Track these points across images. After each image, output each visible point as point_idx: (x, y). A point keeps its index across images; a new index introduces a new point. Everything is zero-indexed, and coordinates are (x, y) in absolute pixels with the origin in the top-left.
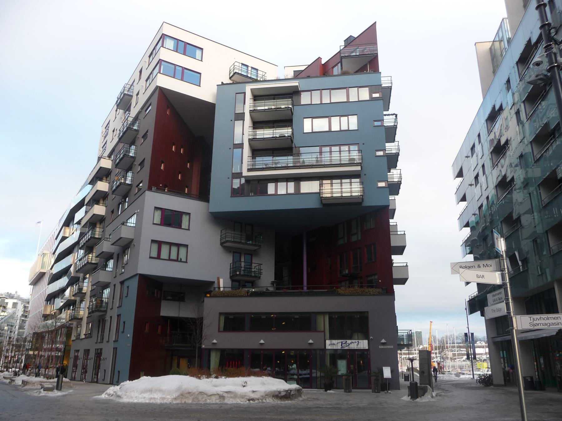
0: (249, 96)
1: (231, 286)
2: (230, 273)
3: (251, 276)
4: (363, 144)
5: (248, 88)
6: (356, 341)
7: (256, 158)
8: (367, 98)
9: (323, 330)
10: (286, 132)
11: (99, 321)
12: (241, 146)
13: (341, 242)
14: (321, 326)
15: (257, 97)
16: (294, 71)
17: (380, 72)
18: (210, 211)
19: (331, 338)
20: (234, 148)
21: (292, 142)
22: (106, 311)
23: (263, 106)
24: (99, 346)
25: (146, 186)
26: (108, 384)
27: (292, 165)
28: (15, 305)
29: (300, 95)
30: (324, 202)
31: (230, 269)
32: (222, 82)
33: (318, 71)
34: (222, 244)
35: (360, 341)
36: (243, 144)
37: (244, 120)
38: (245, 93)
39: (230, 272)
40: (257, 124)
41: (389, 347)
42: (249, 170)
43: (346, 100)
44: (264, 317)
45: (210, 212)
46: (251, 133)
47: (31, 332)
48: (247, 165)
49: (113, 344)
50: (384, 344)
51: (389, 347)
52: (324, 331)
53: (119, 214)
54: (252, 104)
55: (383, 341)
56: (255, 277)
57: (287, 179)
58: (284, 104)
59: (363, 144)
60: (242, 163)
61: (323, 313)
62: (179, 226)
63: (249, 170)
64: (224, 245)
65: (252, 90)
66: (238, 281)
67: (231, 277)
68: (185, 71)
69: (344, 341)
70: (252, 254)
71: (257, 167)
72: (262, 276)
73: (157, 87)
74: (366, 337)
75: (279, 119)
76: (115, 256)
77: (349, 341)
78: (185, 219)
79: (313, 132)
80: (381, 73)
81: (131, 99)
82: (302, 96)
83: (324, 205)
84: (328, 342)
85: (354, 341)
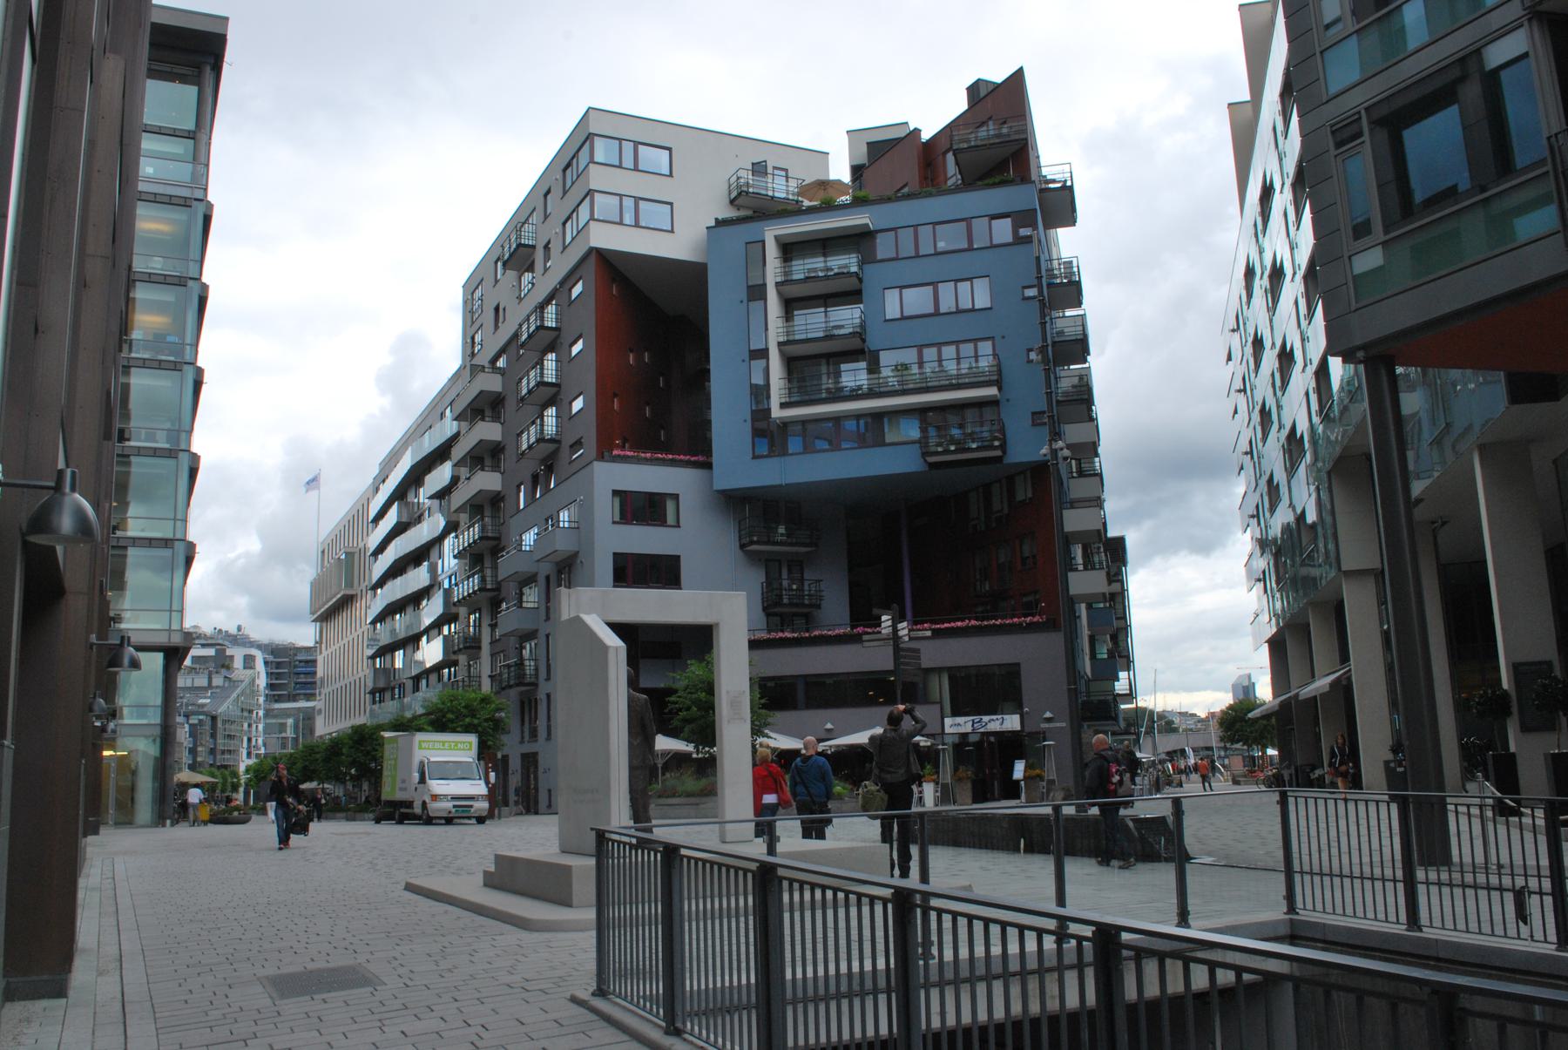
0: (772, 251)
1: (765, 627)
3: (804, 605)
5: (771, 233)
6: (999, 717)
8: (1009, 238)
9: (938, 700)
11: (522, 703)
12: (763, 354)
14: (935, 693)
15: (789, 249)
16: (868, 143)
18: (715, 488)
19: (955, 714)
20: (749, 300)
21: (864, 341)
22: (535, 685)
24: (528, 748)
25: (594, 453)
28: (249, 661)
29: (875, 238)
31: (763, 594)
32: (716, 219)
33: (910, 173)
34: (742, 546)
35: (1005, 717)
36: (767, 350)
37: (765, 300)
38: (763, 242)
40: (790, 305)
41: (1058, 725)
42: (783, 406)
43: (966, 246)
44: (829, 681)
45: (718, 491)
46: (781, 330)
47: (1238, 764)
50: (1049, 720)
51: (1058, 725)
52: (941, 703)
54: (779, 270)
55: (1048, 715)
56: (811, 606)
58: (846, 262)
60: (766, 329)
63: (783, 406)
65: (777, 238)
66: (781, 615)
67: (764, 609)
68: (642, 204)
69: (977, 718)
70: (797, 565)
72: (824, 604)
74: (1018, 707)
75: (834, 291)
76: (541, 580)
77: (986, 718)
78: (670, 506)
79: (903, 318)
81: (533, 253)
82: (878, 241)
84: (948, 721)
85: (994, 717)
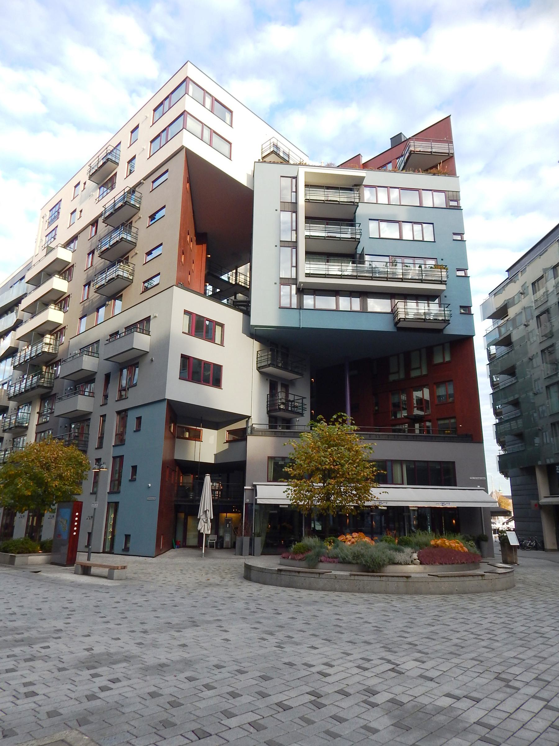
2: (267, 407)
4: (442, 260)
7: (204, 246)
10: (346, 233)
13: (392, 378)
17: (457, 175)
23: (320, 195)
26: (101, 553)
27: (350, 273)
30: (400, 325)
31: (267, 402)
34: (259, 368)
39: (267, 405)
48: (446, 283)
49: (107, 497)
53: (117, 312)
57: (352, 293)
59: (442, 260)
61: (401, 462)
62: (212, 339)
64: (263, 370)
71: (331, 273)
73: (182, 148)
80: (458, 177)
83: (400, 329)
